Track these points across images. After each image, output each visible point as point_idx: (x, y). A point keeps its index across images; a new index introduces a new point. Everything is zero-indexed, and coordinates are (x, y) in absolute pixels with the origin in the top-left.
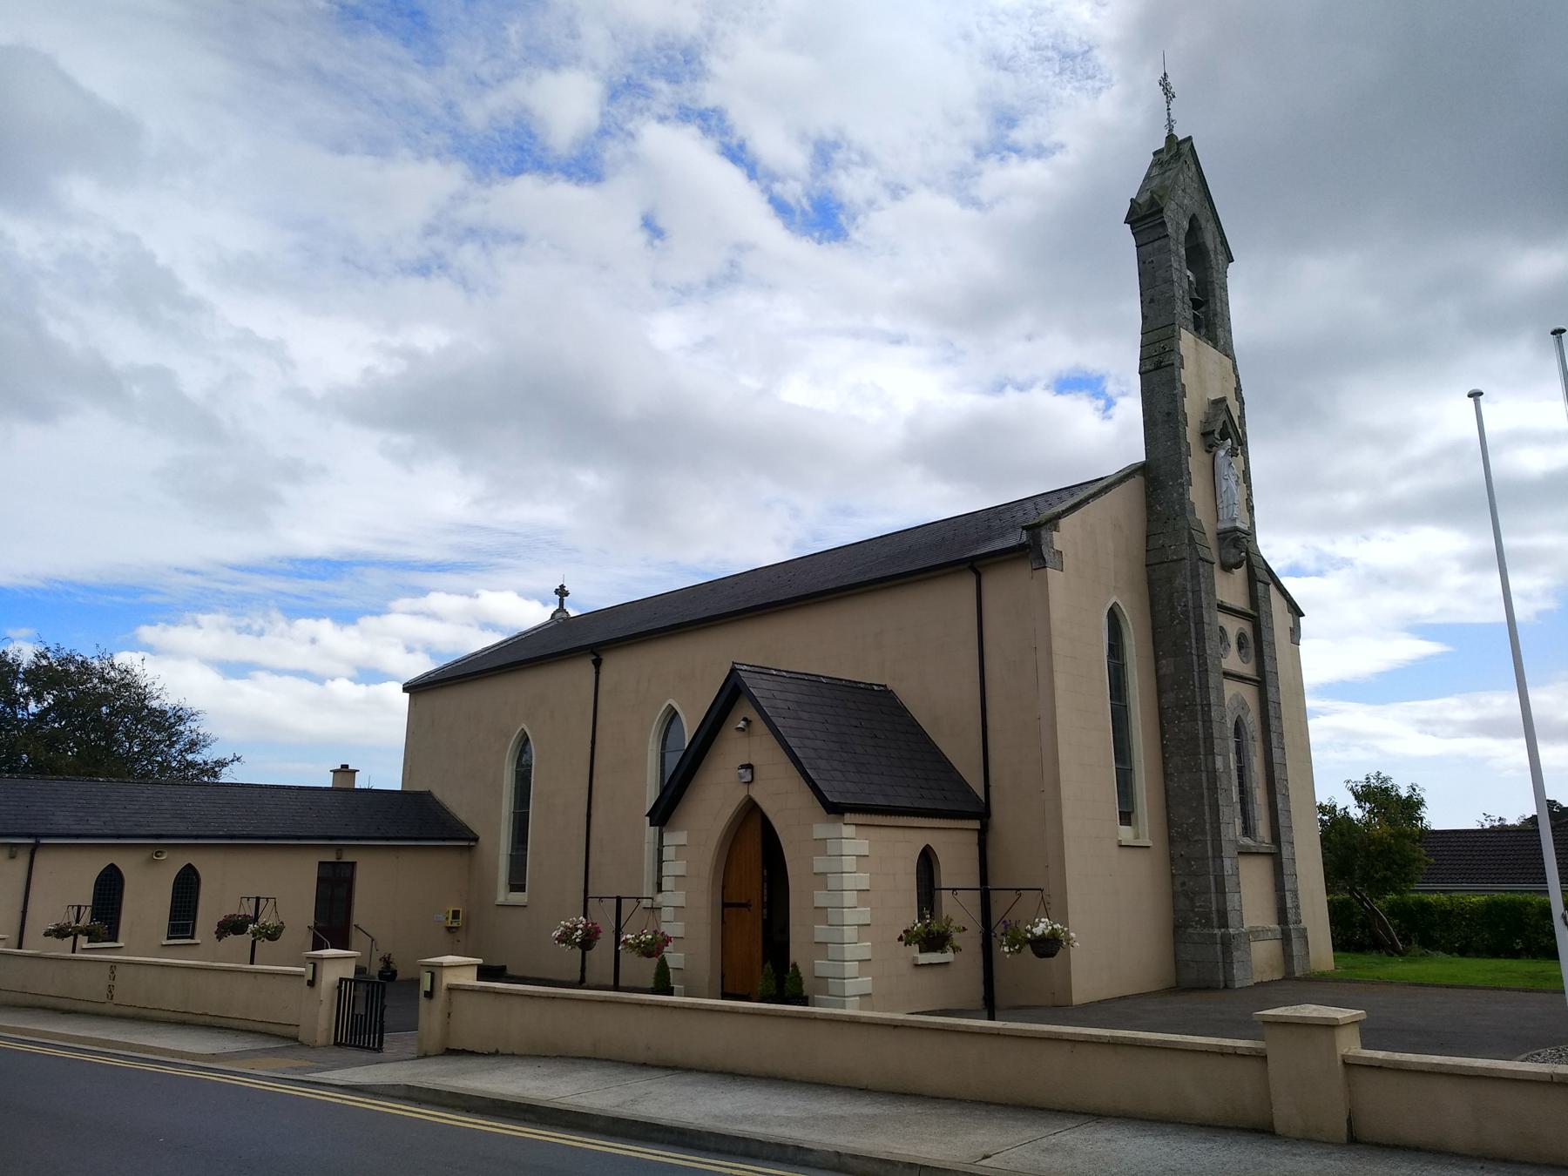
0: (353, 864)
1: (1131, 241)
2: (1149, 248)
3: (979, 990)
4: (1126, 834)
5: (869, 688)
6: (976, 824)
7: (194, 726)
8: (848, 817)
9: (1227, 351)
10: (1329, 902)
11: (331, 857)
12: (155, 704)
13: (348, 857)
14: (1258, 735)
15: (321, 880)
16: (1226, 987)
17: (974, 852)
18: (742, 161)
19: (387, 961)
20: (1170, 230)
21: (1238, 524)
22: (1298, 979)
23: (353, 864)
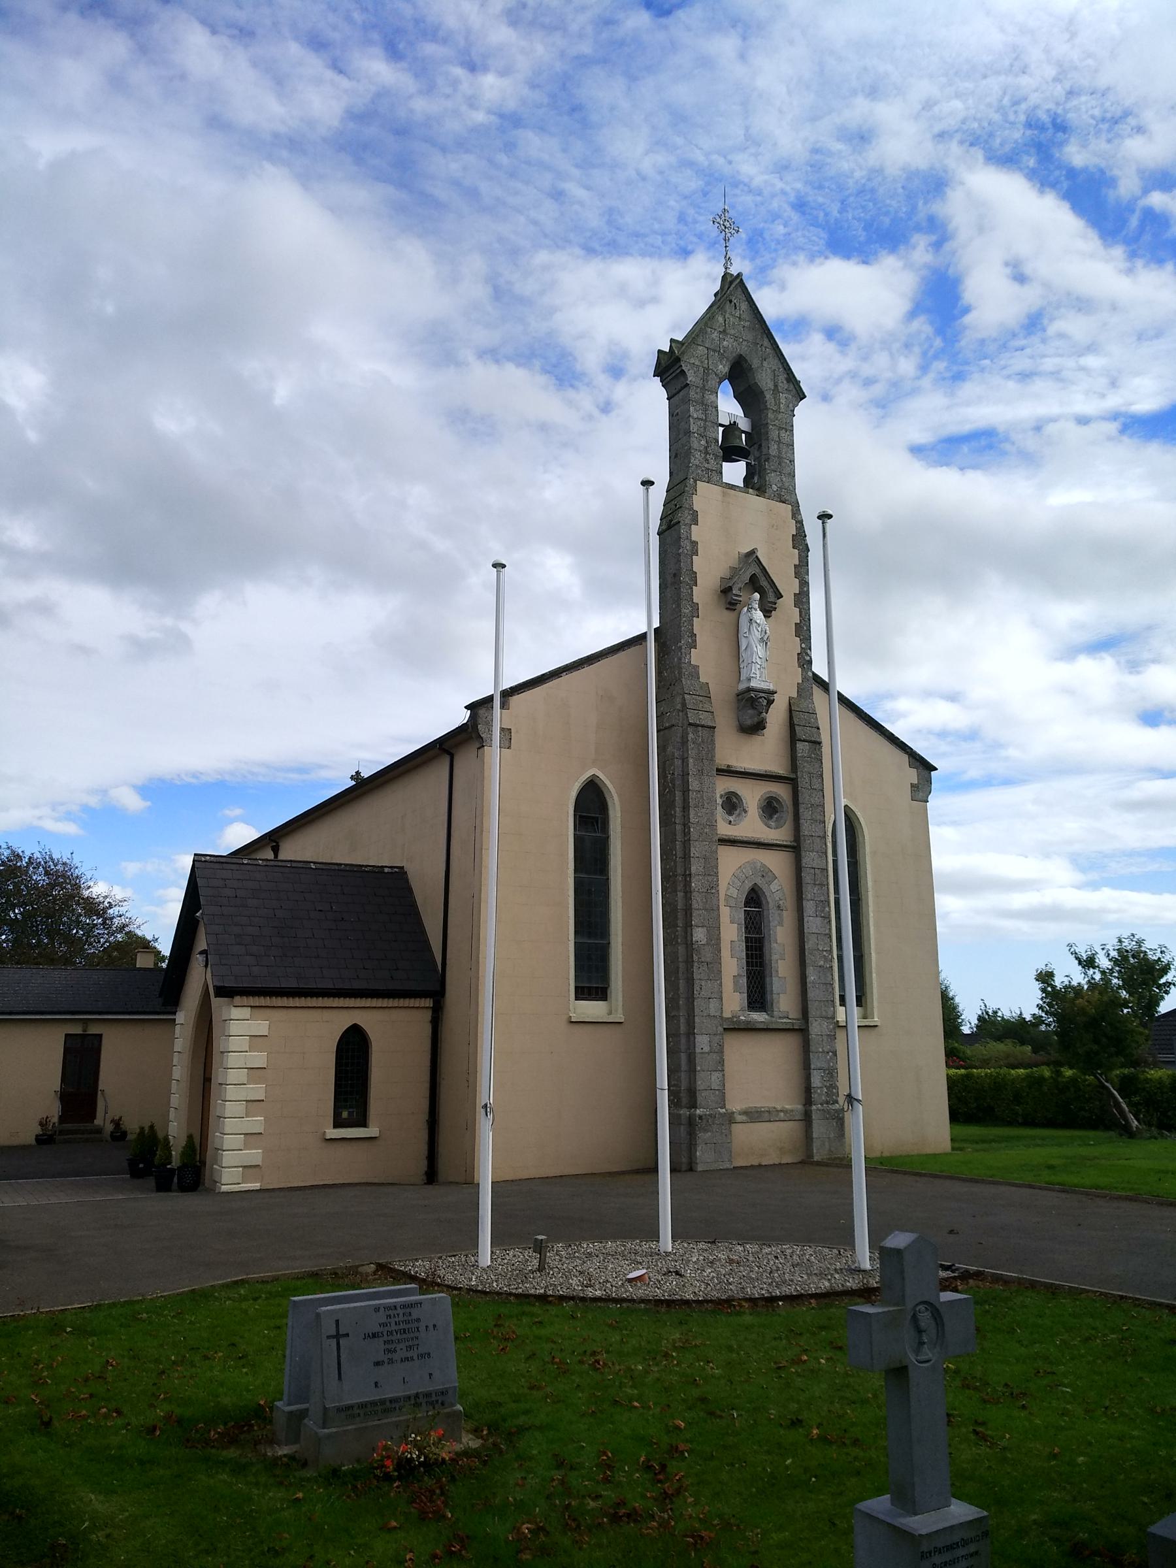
0: (101, 1036)
1: (663, 394)
2: (676, 398)
3: (423, 1165)
4: (593, 1009)
5: (378, 871)
6: (428, 1002)
7: (122, 910)
8: (238, 1000)
9: (787, 496)
10: (952, 1083)
11: (77, 1030)
12: (86, 893)
13: (93, 1030)
14: (789, 903)
15: (67, 1051)
16: (691, 1170)
17: (427, 1030)
18: (706, 325)
19: (117, 1123)
20: (691, 377)
21: (753, 684)
22: (818, 1164)
23: (101, 1036)
